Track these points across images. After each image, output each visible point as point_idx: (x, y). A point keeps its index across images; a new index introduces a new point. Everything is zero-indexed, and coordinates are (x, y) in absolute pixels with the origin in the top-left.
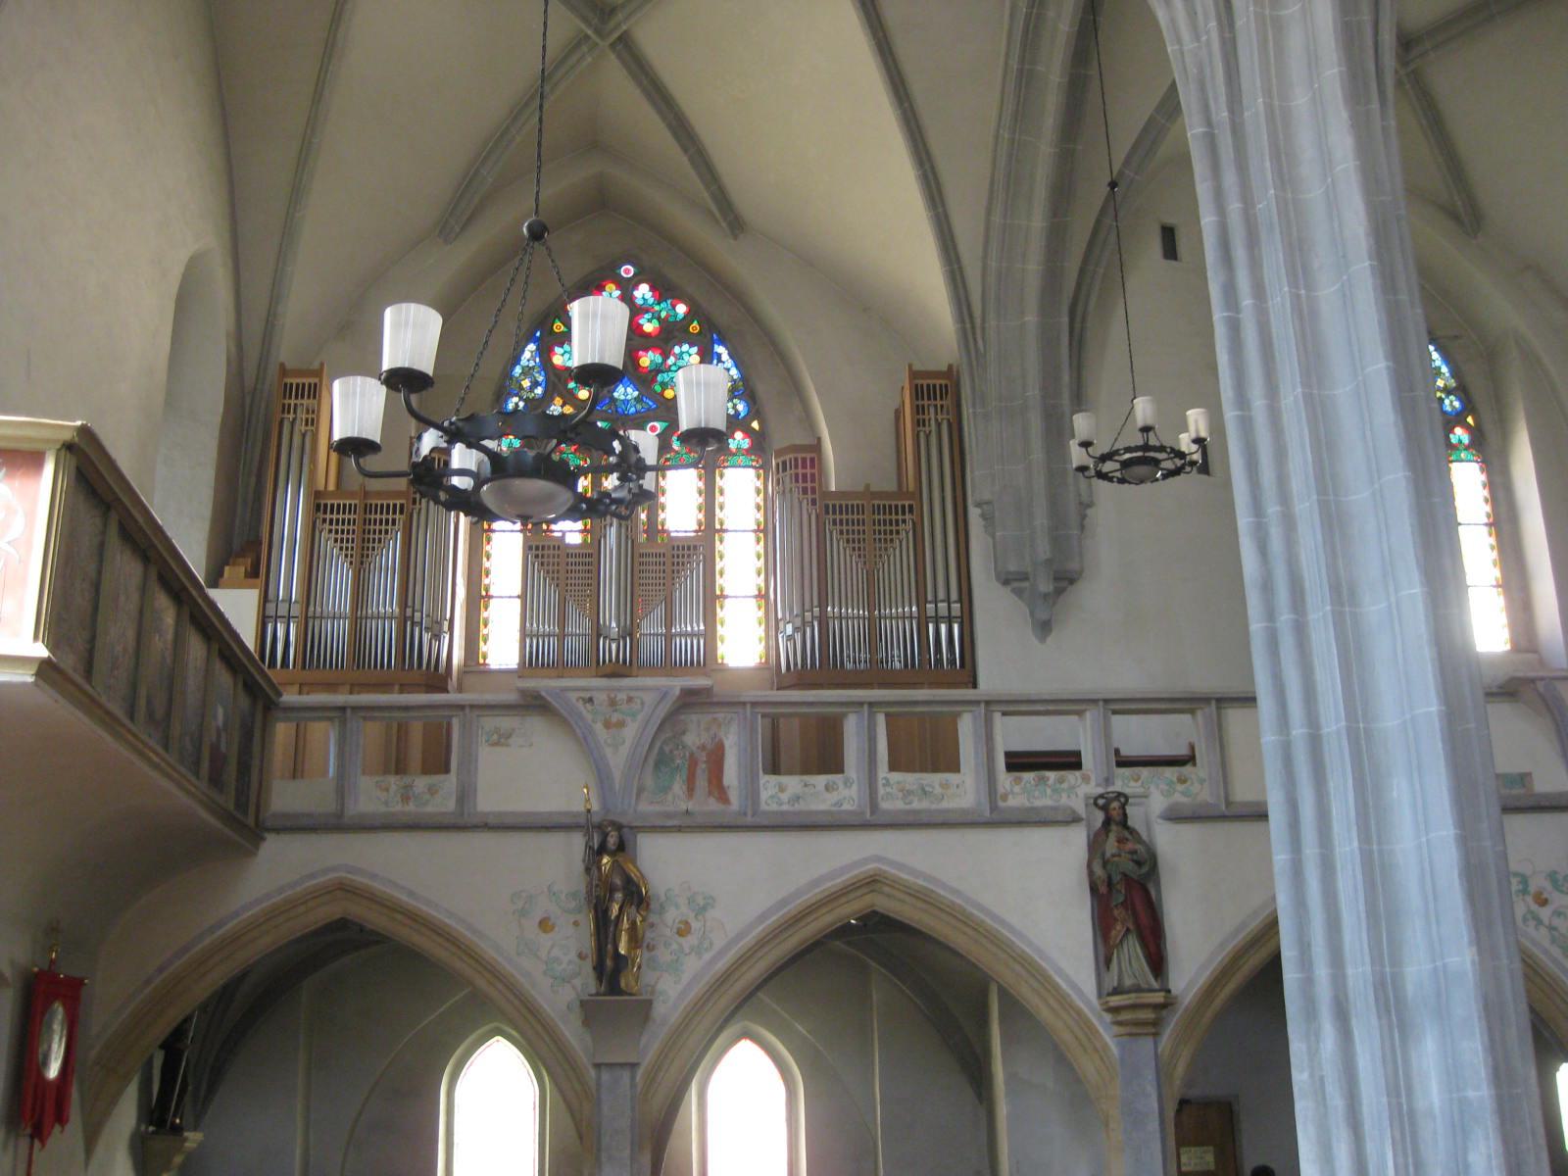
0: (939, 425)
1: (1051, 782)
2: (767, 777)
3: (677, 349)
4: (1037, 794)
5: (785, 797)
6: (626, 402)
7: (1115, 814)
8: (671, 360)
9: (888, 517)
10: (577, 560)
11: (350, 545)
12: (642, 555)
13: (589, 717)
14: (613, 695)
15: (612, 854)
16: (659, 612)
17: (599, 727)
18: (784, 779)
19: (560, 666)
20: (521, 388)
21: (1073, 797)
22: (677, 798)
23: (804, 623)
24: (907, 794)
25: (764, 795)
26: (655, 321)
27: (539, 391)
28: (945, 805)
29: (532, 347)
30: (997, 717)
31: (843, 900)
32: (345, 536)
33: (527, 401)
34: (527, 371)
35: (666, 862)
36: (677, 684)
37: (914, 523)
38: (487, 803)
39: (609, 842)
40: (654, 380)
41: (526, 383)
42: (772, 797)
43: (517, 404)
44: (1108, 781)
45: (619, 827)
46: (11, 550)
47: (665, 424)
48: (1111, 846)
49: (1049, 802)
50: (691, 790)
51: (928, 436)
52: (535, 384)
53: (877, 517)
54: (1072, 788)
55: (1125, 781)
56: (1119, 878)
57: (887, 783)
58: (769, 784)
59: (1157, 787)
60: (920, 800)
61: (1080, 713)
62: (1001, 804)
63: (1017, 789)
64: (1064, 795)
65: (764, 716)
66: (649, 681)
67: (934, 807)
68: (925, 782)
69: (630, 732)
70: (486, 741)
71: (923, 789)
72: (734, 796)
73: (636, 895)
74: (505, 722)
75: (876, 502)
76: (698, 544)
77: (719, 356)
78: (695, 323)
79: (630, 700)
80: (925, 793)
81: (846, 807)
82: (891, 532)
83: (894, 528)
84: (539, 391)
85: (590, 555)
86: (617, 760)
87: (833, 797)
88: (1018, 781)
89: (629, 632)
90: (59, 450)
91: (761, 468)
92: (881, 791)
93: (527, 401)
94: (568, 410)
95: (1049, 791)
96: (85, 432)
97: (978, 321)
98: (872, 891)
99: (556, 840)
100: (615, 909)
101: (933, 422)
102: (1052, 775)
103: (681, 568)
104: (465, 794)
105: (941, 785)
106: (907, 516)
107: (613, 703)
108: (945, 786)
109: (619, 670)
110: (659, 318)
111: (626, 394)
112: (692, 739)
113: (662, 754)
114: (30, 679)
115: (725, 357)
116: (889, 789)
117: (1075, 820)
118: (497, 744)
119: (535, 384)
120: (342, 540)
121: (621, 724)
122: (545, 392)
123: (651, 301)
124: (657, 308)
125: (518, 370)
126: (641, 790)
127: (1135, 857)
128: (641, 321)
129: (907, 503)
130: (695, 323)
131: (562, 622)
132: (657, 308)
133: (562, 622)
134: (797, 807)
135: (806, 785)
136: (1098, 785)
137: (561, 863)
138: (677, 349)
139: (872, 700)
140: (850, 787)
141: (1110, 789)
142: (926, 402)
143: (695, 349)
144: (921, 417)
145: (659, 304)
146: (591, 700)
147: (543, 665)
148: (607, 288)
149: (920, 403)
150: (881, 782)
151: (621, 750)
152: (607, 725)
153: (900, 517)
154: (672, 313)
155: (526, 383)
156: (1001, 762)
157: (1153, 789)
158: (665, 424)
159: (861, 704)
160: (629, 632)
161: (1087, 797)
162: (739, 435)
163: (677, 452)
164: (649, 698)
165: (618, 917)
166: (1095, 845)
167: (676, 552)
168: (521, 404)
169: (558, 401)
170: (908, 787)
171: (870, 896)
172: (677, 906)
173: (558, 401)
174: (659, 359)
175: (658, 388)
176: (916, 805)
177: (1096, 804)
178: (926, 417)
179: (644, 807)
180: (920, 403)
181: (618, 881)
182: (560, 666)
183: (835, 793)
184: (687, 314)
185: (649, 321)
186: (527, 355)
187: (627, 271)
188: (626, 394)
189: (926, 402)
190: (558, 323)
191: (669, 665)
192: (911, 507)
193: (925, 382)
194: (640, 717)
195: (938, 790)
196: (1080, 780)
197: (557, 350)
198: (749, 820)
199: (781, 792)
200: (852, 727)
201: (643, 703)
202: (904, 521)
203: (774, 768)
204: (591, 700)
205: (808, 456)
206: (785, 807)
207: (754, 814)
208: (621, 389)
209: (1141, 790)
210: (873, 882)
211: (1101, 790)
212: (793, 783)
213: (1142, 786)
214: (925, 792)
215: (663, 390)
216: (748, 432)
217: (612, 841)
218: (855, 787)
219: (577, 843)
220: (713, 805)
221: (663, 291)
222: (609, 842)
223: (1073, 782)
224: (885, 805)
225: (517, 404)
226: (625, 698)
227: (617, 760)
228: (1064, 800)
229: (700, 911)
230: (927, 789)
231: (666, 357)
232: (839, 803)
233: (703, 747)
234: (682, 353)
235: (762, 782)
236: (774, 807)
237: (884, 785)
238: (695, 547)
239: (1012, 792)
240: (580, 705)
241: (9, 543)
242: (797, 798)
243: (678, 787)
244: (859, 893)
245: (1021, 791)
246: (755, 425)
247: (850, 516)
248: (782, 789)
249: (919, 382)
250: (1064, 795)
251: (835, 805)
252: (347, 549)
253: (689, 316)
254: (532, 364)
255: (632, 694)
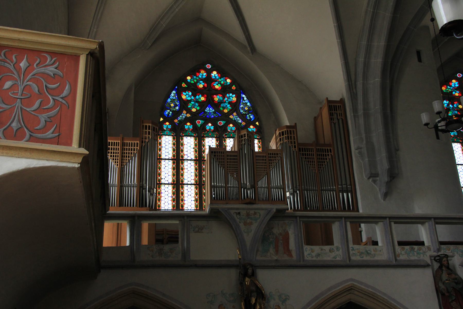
0: (338, 120)
1: (416, 250)
2: (306, 246)
3: (228, 95)
4: (411, 254)
5: (314, 254)
6: (210, 113)
7: (445, 263)
8: (226, 99)
9: (322, 153)
10: (230, 157)
11: (117, 158)
12: (257, 156)
13: (238, 220)
14: (248, 212)
15: (249, 277)
16: (265, 179)
17: (242, 225)
18: (314, 247)
19: (226, 199)
20: (171, 107)
21: (425, 256)
22: (272, 255)
23: (294, 192)
24: (361, 253)
25: (306, 254)
26: (219, 85)
27: (177, 108)
28: (376, 258)
29: (174, 92)
30: (393, 225)
31: (339, 297)
32: (115, 155)
33: (173, 111)
34: (173, 101)
35: (268, 280)
36: (274, 207)
37: (332, 156)
38: (195, 256)
39: (246, 270)
40: (220, 106)
41: (172, 105)
42: (309, 254)
43: (169, 113)
44: (439, 250)
45: (252, 266)
46: (64, 102)
47: (224, 122)
48: (445, 276)
49: (416, 258)
50: (277, 252)
51: (335, 124)
52: (176, 105)
53: (318, 153)
54: (424, 252)
55: (445, 250)
56: (452, 289)
57: (353, 249)
58: (307, 249)
59: (457, 253)
60: (366, 256)
61: (422, 223)
62: (398, 258)
63: (403, 252)
64: (422, 255)
65: (303, 222)
66: (263, 206)
67: (372, 259)
68: (367, 249)
69: (254, 227)
70: (193, 231)
71: (367, 252)
72: (294, 254)
73: (261, 294)
74: (201, 223)
75: (318, 148)
76: (278, 152)
77: (243, 98)
78: (234, 86)
79: (255, 213)
80: (368, 253)
81: (338, 259)
82: (322, 159)
83: (325, 157)
84: (177, 108)
85: (236, 156)
86: (248, 239)
87: (333, 255)
88: (403, 249)
89: (254, 186)
90: (87, 55)
91: (260, 139)
92: (351, 252)
93: (173, 111)
94: (188, 115)
95: (415, 253)
96: (102, 42)
97: (353, 82)
98: (351, 293)
99: (224, 271)
100: (253, 301)
101: (336, 119)
102: (416, 247)
103: (272, 162)
104: (185, 253)
105: (374, 251)
106: (329, 153)
107: (248, 215)
108: (375, 250)
109: (251, 202)
110: (221, 84)
111: (210, 110)
112: (276, 231)
113: (265, 238)
114: (77, 166)
115: (245, 99)
116: (354, 252)
117: (426, 266)
118: (198, 232)
119: (176, 105)
120: (114, 156)
121: (251, 224)
122: (179, 108)
123: (218, 77)
124: (220, 80)
125: (169, 100)
126: (258, 251)
127: (456, 281)
128: (214, 85)
129: (329, 148)
130: (234, 86)
131: (227, 182)
132: (220, 80)
133: (227, 182)
134: (319, 259)
135: (322, 250)
136: (434, 252)
137: (227, 281)
138: (228, 95)
139: (345, 216)
140: (339, 251)
141: (439, 253)
142: (333, 112)
143: (234, 96)
144: (332, 117)
145: (220, 78)
146: (239, 213)
147: (219, 199)
148: (201, 72)
149: (331, 112)
150: (350, 249)
151: (250, 234)
152: (245, 224)
153: (327, 153)
154: (225, 82)
155: (172, 105)
156: (396, 243)
157: (455, 253)
158: (224, 122)
159: (341, 217)
160: (254, 186)
161: (431, 257)
162: (252, 127)
163: (229, 132)
164: (262, 212)
165: (255, 304)
166: (437, 278)
167: (270, 156)
168: (171, 113)
169: (185, 112)
170: (361, 251)
171: (349, 295)
172: (274, 300)
173: (185, 112)
174: (221, 98)
175: (221, 109)
176: (366, 258)
177: (435, 259)
178: (334, 117)
179: (259, 258)
180: (331, 112)
181: (253, 288)
182: (226, 199)
183: (333, 253)
184: (231, 83)
185: (217, 85)
186: (172, 95)
187: (209, 66)
188: (210, 110)
189: (333, 112)
190: (183, 83)
191: (270, 200)
192: (330, 150)
193: (333, 104)
194: (258, 221)
195: (373, 253)
196: (427, 249)
197: (184, 93)
198: (302, 263)
199: (311, 252)
200: (336, 228)
201: (260, 215)
202: (328, 155)
203: (309, 242)
204: (239, 213)
205: (292, 130)
206: (314, 259)
207: (303, 261)
208: (208, 109)
209: (451, 254)
210: (350, 289)
211: (435, 254)
212: (317, 249)
213: (451, 252)
214: (368, 253)
215: (223, 110)
216: (255, 126)
217: (250, 271)
218: (341, 250)
219: (233, 274)
220: (286, 258)
221: (223, 74)
222: (246, 270)
223: (424, 250)
224: (353, 258)
225: (169, 113)
226: (253, 213)
227: (248, 239)
228: (422, 257)
229: (284, 301)
230: (369, 252)
231: (224, 98)
232: (335, 257)
233: (281, 234)
234: (230, 96)
235: (304, 248)
236: (310, 258)
237: (352, 250)
238: (277, 154)
239: (401, 254)
240: (235, 215)
241: (61, 98)
242: (318, 255)
243: (272, 251)
244: (345, 294)
245: (404, 254)
246: (257, 123)
247: (308, 153)
248: (313, 251)
249: (331, 104)
250: (422, 255)
251: (334, 258)
252: (116, 159)
253: (231, 84)
254: (174, 98)
255: (256, 211)
